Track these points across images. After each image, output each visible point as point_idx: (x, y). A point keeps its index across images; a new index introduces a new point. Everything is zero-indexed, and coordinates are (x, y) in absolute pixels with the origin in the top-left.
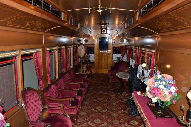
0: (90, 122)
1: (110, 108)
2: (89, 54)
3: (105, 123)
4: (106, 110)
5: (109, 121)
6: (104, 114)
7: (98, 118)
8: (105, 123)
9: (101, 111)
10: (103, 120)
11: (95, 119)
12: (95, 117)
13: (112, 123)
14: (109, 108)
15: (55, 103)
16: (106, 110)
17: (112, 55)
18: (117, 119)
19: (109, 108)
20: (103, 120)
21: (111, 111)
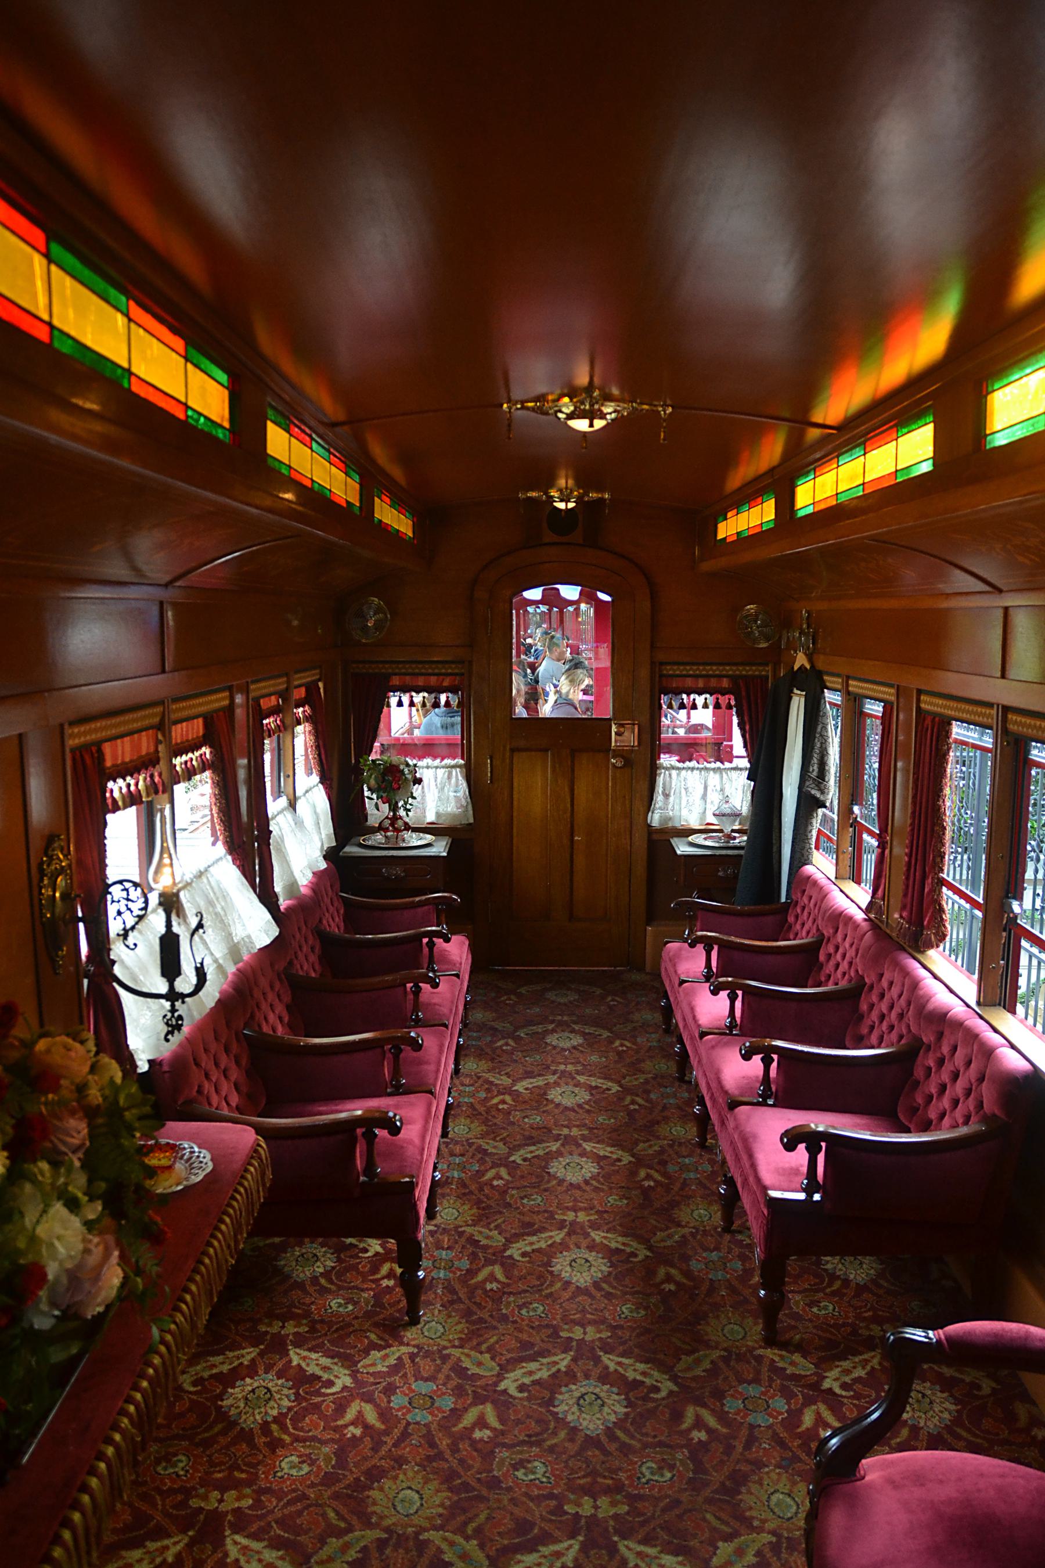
0: (636, 1255)
1: (490, 1174)
2: (932, 425)
3: (522, 1388)
4: (515, 1251)
5: (503, 1172)
6: (534, 1133)
7: (578, 1187)
8: (522, 1388)
9: (564, 1361)
10: (540, 1177)
11: (620, 1424)
12: (625, 1450)
13: (459, 1392)
14: (498, 1177)
15: (163, 314)
16: (516, 1157)
17: (197, 717)
18: (405, 1435)
19: (498, 1177)
20: (540, 1277)
21: (475, 1243)
